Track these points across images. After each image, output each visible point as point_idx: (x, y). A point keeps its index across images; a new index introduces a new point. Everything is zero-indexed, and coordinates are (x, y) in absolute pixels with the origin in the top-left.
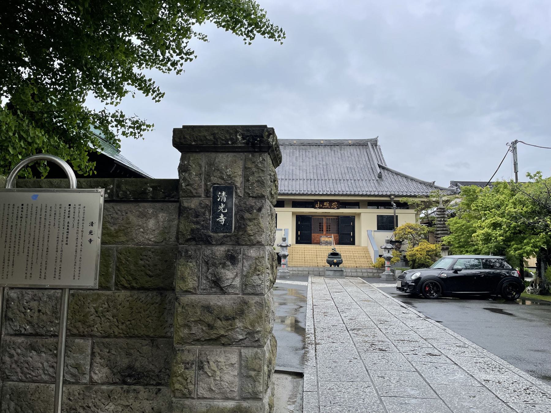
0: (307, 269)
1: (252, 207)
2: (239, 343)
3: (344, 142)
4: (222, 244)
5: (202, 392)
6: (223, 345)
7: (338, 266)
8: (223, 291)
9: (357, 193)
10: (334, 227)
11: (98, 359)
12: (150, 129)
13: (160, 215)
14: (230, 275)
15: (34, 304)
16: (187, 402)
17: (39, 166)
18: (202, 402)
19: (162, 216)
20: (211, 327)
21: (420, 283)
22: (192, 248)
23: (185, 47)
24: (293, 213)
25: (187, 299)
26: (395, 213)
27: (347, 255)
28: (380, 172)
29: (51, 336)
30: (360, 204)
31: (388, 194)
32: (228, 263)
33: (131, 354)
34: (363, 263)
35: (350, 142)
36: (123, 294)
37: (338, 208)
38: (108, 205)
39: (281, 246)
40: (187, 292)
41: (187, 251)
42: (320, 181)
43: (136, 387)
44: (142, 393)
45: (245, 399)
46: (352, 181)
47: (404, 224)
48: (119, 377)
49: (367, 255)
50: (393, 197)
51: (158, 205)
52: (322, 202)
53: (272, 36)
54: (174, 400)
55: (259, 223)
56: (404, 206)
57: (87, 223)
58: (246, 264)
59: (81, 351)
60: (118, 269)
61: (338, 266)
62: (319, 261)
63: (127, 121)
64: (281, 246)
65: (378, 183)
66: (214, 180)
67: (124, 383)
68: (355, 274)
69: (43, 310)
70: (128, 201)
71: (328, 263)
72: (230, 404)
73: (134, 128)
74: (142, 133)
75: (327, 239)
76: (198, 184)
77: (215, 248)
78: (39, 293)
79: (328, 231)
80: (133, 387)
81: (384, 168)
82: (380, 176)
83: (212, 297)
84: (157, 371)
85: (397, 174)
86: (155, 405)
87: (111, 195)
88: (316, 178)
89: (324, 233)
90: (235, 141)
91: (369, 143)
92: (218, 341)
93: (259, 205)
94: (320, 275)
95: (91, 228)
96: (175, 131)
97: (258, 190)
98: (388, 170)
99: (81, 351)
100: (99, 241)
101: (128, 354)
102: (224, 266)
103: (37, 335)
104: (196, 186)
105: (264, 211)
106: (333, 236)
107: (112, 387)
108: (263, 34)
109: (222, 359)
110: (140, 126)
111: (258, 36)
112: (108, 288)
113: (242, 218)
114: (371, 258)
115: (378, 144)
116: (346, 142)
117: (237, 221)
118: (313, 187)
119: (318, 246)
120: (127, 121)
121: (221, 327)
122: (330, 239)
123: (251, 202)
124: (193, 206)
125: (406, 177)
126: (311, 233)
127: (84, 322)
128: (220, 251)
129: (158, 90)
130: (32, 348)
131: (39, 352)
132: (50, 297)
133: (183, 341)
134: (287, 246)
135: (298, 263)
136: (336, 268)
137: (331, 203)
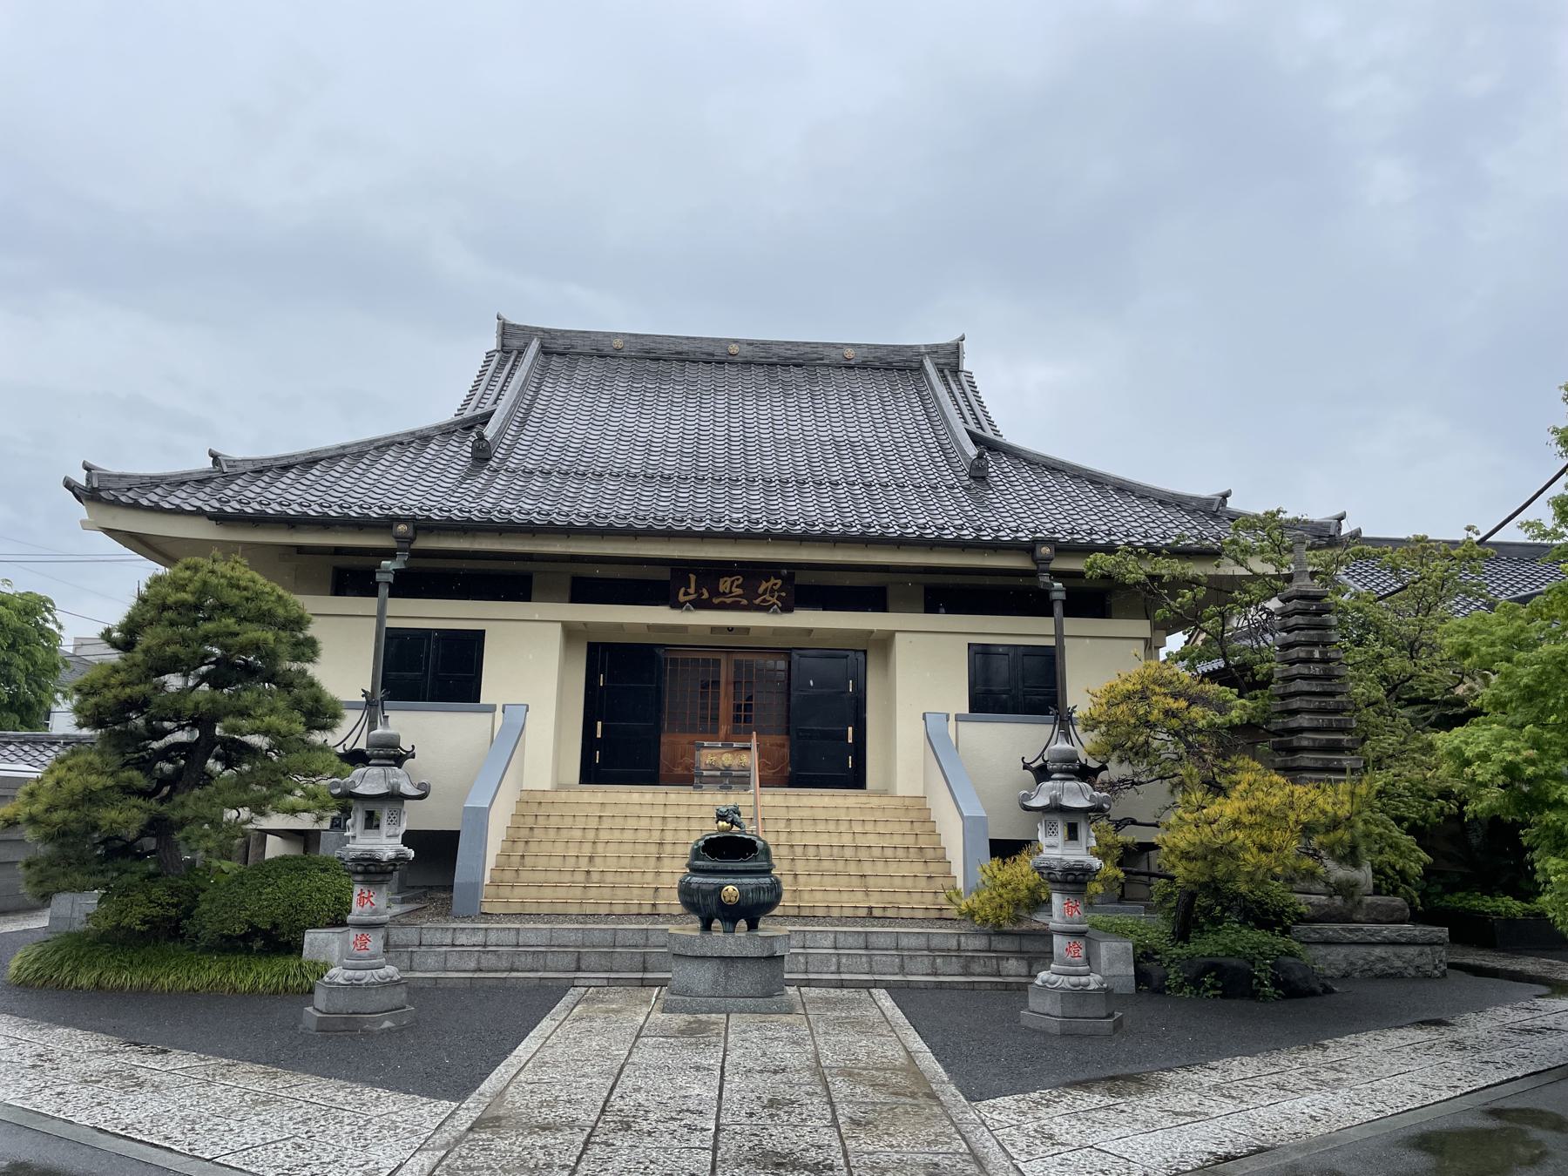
7: (752, 926)
27: (823, 840)
30: (891, 593)
35: (849, 353)
37: (787, 608)
47: (1100, 684)
49: (923, 842)
50: (1045, 550)
52: (711, 572)
56: (1094, 599)
61: (752, 926)
75: (727, 759)
79: (744, 719)
82: (979, 475)
85: (1055, 468)
89: (724, 729)
106: (754, 743)
114: (943, 860)
115: (966, 365)
116: (834, 354)
122: (745, 758)
136: (738, 940)
137: (752, 583)
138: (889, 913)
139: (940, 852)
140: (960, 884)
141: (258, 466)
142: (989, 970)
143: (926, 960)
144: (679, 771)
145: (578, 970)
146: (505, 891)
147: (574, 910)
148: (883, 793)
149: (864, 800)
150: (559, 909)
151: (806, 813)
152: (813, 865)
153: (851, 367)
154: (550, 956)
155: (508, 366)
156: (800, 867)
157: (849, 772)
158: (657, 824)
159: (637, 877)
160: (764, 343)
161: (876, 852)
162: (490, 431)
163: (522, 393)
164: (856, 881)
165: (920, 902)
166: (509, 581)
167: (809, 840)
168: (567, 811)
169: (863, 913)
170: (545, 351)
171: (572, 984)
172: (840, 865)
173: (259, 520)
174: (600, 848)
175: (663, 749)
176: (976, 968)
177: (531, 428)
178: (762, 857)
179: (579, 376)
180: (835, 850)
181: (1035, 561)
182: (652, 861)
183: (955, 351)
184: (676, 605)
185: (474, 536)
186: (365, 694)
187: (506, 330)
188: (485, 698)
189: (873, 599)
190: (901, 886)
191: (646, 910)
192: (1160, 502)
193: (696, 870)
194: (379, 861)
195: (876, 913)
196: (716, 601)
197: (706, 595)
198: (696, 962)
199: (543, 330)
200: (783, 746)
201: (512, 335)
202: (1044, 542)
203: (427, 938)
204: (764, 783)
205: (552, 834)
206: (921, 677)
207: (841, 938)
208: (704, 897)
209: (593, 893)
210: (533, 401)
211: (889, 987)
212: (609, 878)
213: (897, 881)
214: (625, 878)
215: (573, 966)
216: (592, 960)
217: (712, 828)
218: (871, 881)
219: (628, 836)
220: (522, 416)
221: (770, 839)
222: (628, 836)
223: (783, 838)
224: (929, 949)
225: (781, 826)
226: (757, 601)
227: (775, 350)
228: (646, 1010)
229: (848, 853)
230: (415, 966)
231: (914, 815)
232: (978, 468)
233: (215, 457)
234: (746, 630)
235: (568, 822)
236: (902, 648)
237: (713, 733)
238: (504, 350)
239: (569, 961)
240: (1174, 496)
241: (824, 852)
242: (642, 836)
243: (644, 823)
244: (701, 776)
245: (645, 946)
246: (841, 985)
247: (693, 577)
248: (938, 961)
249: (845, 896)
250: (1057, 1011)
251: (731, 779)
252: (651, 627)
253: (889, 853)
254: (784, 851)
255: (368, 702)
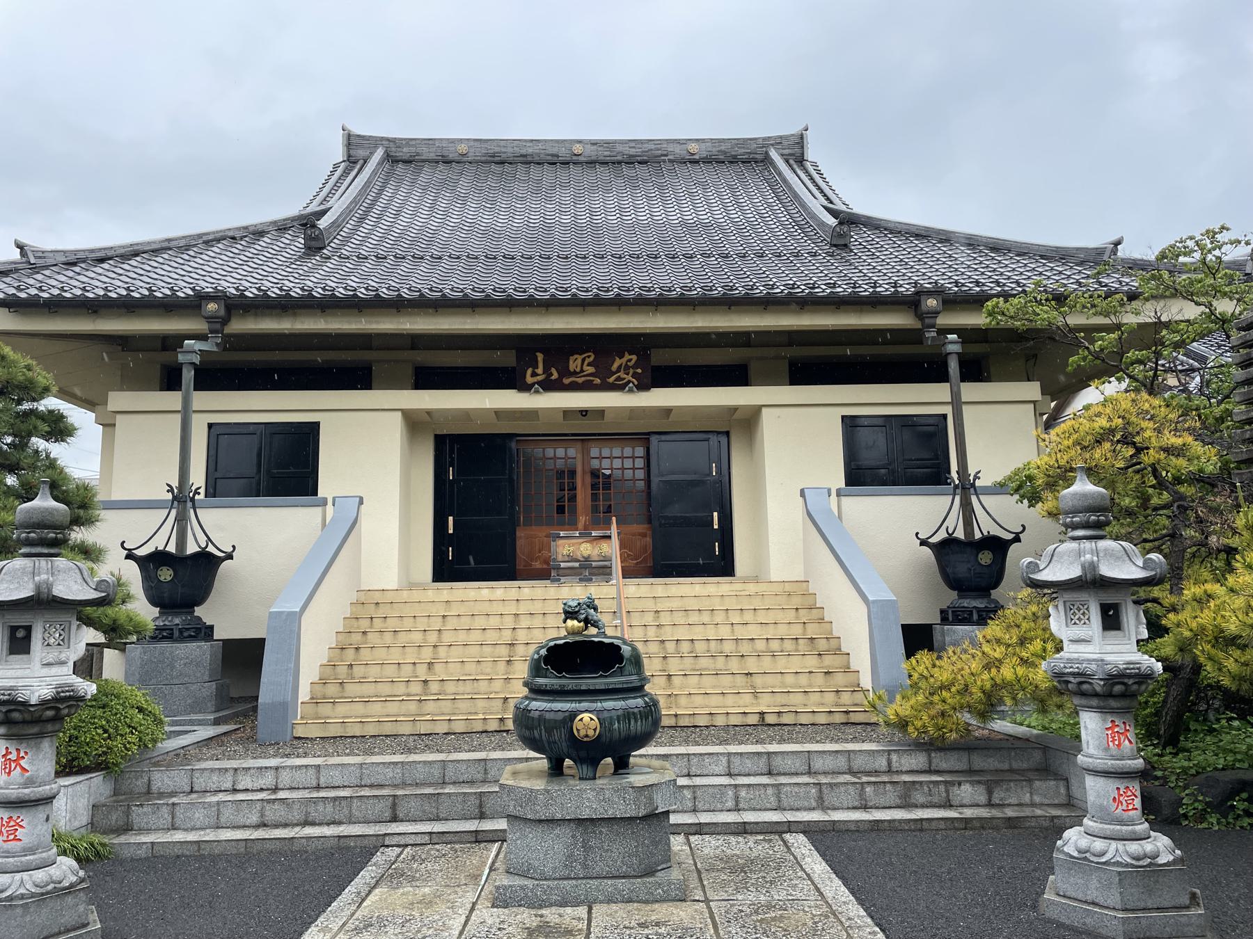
3: (671, 148)
27: (698, 633)
31: (906, 289)
35: (693, 148)
37: (643, 387)
49: (812, 631)
50: (932, 303)
61: (622, 765)
75: (586, 549)
79: (601, 516)
89: (582, 520)
91: (774, 154)
115: (811, 155)
116: (678, 151)
126: (514, 524)
137: (603, 357)
138: (786, 719)
139: (833, 643)
140: (866, 681)
141: (72, 258)
142: (936, 800)
143: (851, 789)
144: (537, 565)
145: (394, 819)
146: (325, 710)
147: (406, 729)
148: (756, 580)
149: (738, 586)
150: (388, 729)
151: (675, 604)
152: (688, 662)
153: (696, 162)
154: (356, 803)
155: (354, 173)
156: (674, 666)
158: (509, 622)
159: (483, 686)
160: (607, 142)
161: (761, 645)
162: (323, 223)
163: (360, 193)
164: (740, 680)
165: (818, 704)
166: (346, 367)
167: (682, 634)
168: (408, 611)
169: (753, 720)
170: (391, 159)
171: (381, 842)
172: (720, 662)
173: (56, 306)
174: (442, 652)
175: (518, 543)
176: (919, 798)
177: (369, 222)
178: (629, 668)
179: (423, 178)
180: (713, 644)
181: (920, 316)
182: (502, 666)
183: (800, 140)
184: (525, 388)
185: (295, 315)
186: (171, 490)
187: (352, 141)
188: (322, 491)
189: (736, 376)
190: (793, 686)
191: (493, 726)
192: (1042, 257)
193: (537, 692)
194: (25, 704)
195: (770, 719)
196: (566, 381)
197: (555, 375)
198: (540, 828)
199: (388, 140)
200: (644, 535)
201: (359, 146)
202: (930, 293)
203: (200, 783)
204: (627, 574)
205: (388, 638)
206: (792, 448)
207: (736, 761)
208: (549, 731)
209: (430, 707)
210: (375, 201)
211: (808, 830)
212: (451, 688)
213: (790, 679)
214: (468, 687)
215: (387, 814)
216: (413, 807)
217: (558, 631)
218: (758, 680)
219: (476, 636)
220: (361, 210)
221: (634, 635)
222: (476, 636)
223: (651, 633)
224: (851, 772)
225: (649, 619)
226: (611, 380)
227: (619, 148)
228: (471, 897)
229: (728, 647)
230: (178, 822)
231: (796, 601)
232: (840, 235)
234: (600, 413)
235: (408, 624)
236: (769, 422)
237: (573, 525)
238: (351, 160)
239: (383, 808)
240: (1057, 249)
241: (700, 647)
242: (491, 637)
243: (494, 622)
244: (559, 568)
245: (484, 781)
246: (743, 829)
247: (540, 357)
248: (868, 789)
249: (730, 700)
250: (1114, 898)
251: (592, 571)
252: (499, 414)
253: (775, 645)
254: (653, 648)
255: (175, 498)
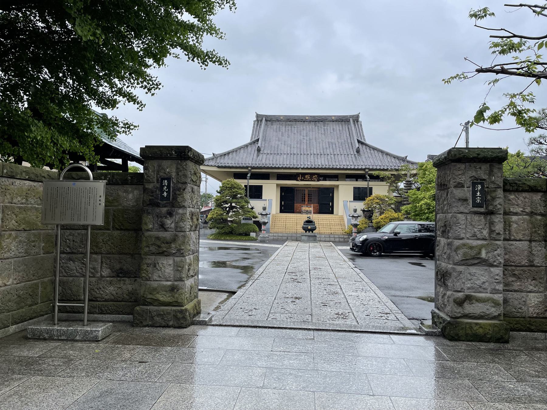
0: (286, 235)
1: (180, 188)
2: (173, 255)
4: (165, 207)
5: (155, 277)
6: (166, 256)
8: (166, 230)
9: (335, 167)
10: (315, 198)
11: (104, 265)
12: (136, 129)
13: (135, 192)
14: (169, 222)
15: (71, 237)
16: (148, 282)
17: (64, 159)
18: (155, 282)
19: (136, 192)
20: (159, 247)
21: (365, 244)
22: (150, 209)
23: (155, 81)
24: (277, 185)
25: (147, 234)
26: (368, 185)
28: (358, 147)
29: (80, 253)
31: (364, 167)
32: (168, 216)
33: (121, 263)
34: (338, 230)
35: (333, 118)
36: (116, 233)
38: (107, 186)
39: (261, 214)
40: (148, 230)
41: (147, 210)
42: (302, 156)
43: (124, 279)
44: (127, 281)
45: (176, 281)
46: (332, 156)
48: (115, 273)
50: (367, 170)
51: (134, 186)
52: (304, 175)
53: (221, 64)
54: (142, 281)
55: (183, 197)
57: (98, 196)
58: (177, 217)
59: (96, 261)
60: (113, 220)
62: (298, 228)
63: (120, 123)
64: (261, 214)
65: (356, 158)
66: (161, 174)
67: (118, 276)
68: (328, 239)
69: (76, 240)
70: (118, 184)
71: (304, 229)
72: (169, 283)
73: (125, 128)
74: (131, 131)
75: (307, 209)
76: (153, 176)
77: (161, 209)
78: (73, 232)
79: (310, 201)
80: (123, 278)
81: (362, 143)
82: (358, 151)
83: (160, 233)
84: (134, 270)
85: (374, 149)
86: (134, 287)
87: (109, 181)
88: (299, 153)
89: (306, 203)
90: (172, 154)
92: (163, 254)
93: (184, 187)
94: (297, 240)
95: (100, 198)
96: (141, 148)
97: (183, 180)
98: (366, 145)
99: (96, 261)
100: (104, 204)
101: (120, 262)
102: (166, 217)
103: (72, 253)
104: (152, 177)
105: (186, 190)
107: (112, 279)
108: (214, 62)
109: (165, 262)
110: (130, 126)
111: (210, 64)
112: (109, 229)
113: (175, 194)
115: (360, 120)
117: (173, 195)
118: (295, 162)
119: (298, 215)
120: (120, 123)
121: (164, 248)
123: (180, 185)
124: (150, 187)
125: (382, 152)
127: (97, 246)
128: (164, 210)
129: (141, 102)
130: (70, 259)
131: (74, 261)
132: (79, 234)
133: (146, 254)
134: (267, 214)
135: (280, 230)
148: (337, 215)
156: (320, 227)
157: (331, 211)
166: (266, 176)
170: (266, 121)
184: (297, 180)
233: (214, 154)
238: (258, 120)
251: (308, 212)
